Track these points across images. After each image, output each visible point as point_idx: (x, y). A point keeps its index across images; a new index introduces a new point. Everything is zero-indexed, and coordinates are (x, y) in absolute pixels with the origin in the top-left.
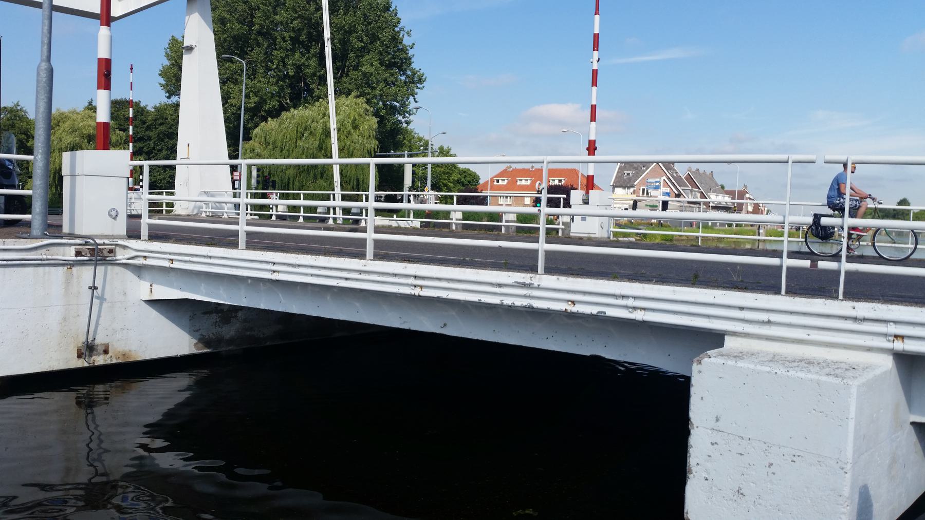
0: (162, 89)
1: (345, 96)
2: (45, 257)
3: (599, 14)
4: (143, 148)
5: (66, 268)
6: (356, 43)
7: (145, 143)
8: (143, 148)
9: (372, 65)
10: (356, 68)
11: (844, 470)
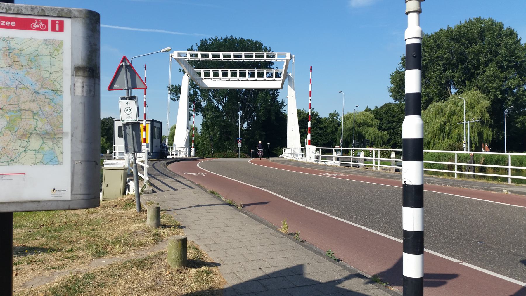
1: (468, 91)
4: (391, 127)
7: (392, 124)
8: (391, 127)
11: (310, 159)
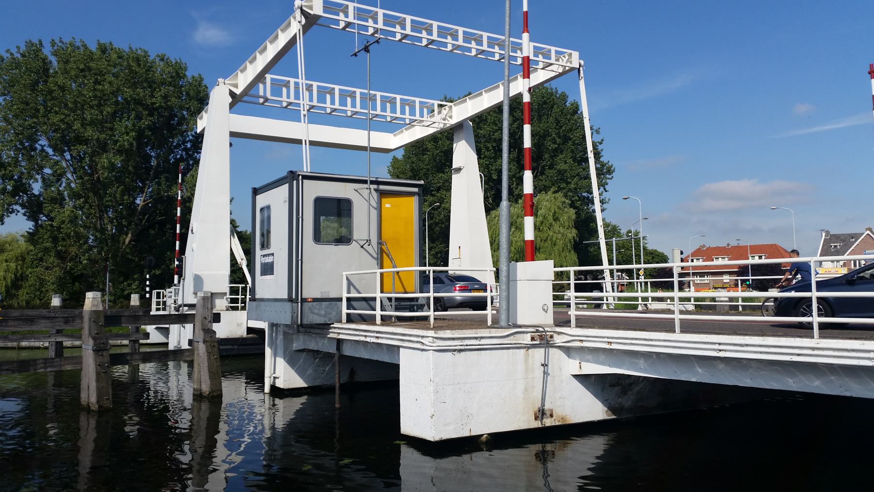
2: (514, 342)
3: (528, 32)
5: (525, 350)
6: (550, 145)
9: (566, 162)
10: (551, 167)
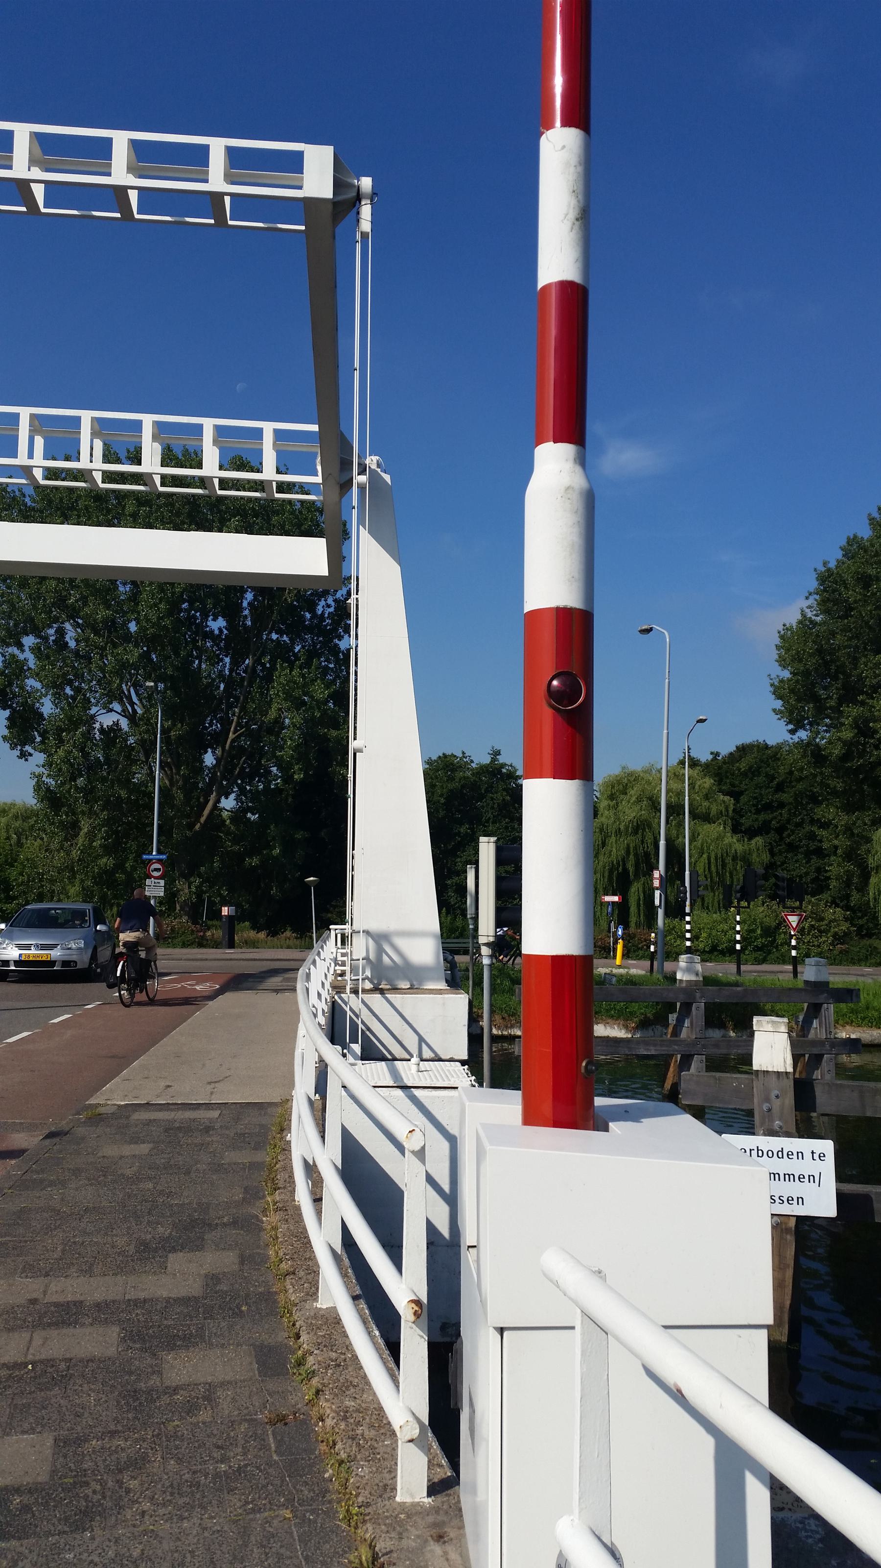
0: (779, 719)
4: (770, 821)
